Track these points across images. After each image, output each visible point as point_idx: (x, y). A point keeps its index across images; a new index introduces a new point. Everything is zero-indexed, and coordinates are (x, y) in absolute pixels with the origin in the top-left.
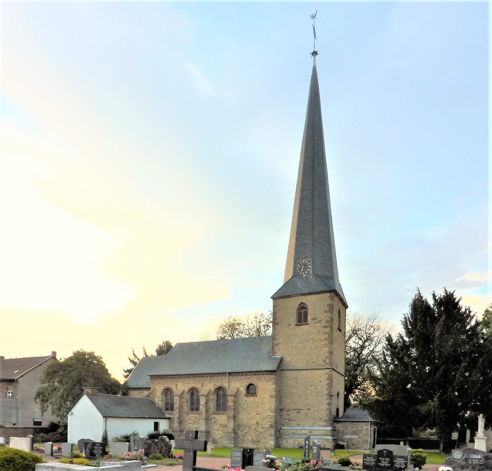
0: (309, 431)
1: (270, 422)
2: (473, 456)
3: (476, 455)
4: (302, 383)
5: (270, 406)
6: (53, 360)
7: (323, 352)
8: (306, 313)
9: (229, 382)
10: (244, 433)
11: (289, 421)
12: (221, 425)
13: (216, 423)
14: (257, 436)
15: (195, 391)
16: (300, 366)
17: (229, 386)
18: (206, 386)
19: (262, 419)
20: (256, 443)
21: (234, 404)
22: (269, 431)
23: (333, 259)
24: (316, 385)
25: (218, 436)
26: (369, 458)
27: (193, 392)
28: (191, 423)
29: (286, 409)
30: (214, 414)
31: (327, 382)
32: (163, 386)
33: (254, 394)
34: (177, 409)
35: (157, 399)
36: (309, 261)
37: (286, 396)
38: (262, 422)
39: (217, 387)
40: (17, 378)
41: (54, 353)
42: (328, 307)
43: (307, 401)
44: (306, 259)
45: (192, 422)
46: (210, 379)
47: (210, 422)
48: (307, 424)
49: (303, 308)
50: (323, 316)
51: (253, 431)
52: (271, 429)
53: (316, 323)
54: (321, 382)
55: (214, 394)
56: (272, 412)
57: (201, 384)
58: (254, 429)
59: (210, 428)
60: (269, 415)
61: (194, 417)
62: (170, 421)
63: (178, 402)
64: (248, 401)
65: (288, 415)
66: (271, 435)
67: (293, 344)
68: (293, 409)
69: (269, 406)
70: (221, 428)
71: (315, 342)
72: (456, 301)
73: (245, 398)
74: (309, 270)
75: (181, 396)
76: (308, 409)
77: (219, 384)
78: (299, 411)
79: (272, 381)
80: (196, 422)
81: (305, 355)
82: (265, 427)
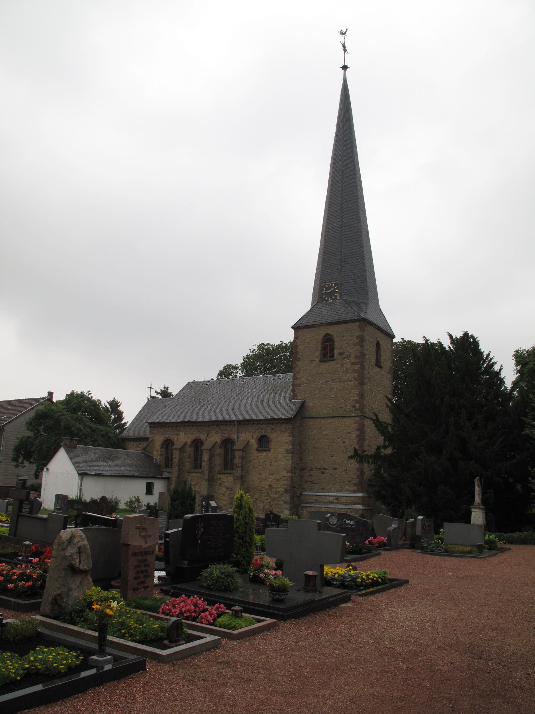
1: (284, 485)
4: (326, 435)
5: (286, 464)
6: (47, 403)
7: (352, 395)
8: (332, 347)
11: (312, 483)
12: (227, 488)
13: (222, 486)
14: (270, 503)
15: (199, 444)
17: (238, 438)
18: (211, 437)
19: (275, 480)
21: (242, 461)
23: (368, 280)
24: (344, 437)
27: (197, 444)
29: (308, 468)
30: (219, 473)
31: (358, 432)
32: (163, 436)
34: (176, 466)
36: (336, 284)
37: (308, 451)
38: (275, 485)
39: (224, 438)
40: (3, 424)
41: (51, 394)
42: (357, 339)
43: (333, 458)
44: (333, 281)
46: (217, 429)
47: (214, 484)
48: (333, 489)
50: (352, 351)
51: (264, 496)
53: (343, 359)
54: (349, 433)
55: (220, 447)
56: (287, 472)
57: (206, 435)
58: (266, 493)
59: (215, 491)
60: (283, 475)
61: (196, 477)
62: (168, 481)
63: (178, 457)
64: (259, 456)
65: (311, 476)
66: (285, 503)
69: (284, 463)
70: (228, 492)
71: (342, 383)
72: (123, 422)
73: (256, 454)
75: (182, 450)
77: (227, 434)
78: (324, 470)
79: (288, 431)
80: (198, 484)
81: (331, 398)
82: (280, 491)
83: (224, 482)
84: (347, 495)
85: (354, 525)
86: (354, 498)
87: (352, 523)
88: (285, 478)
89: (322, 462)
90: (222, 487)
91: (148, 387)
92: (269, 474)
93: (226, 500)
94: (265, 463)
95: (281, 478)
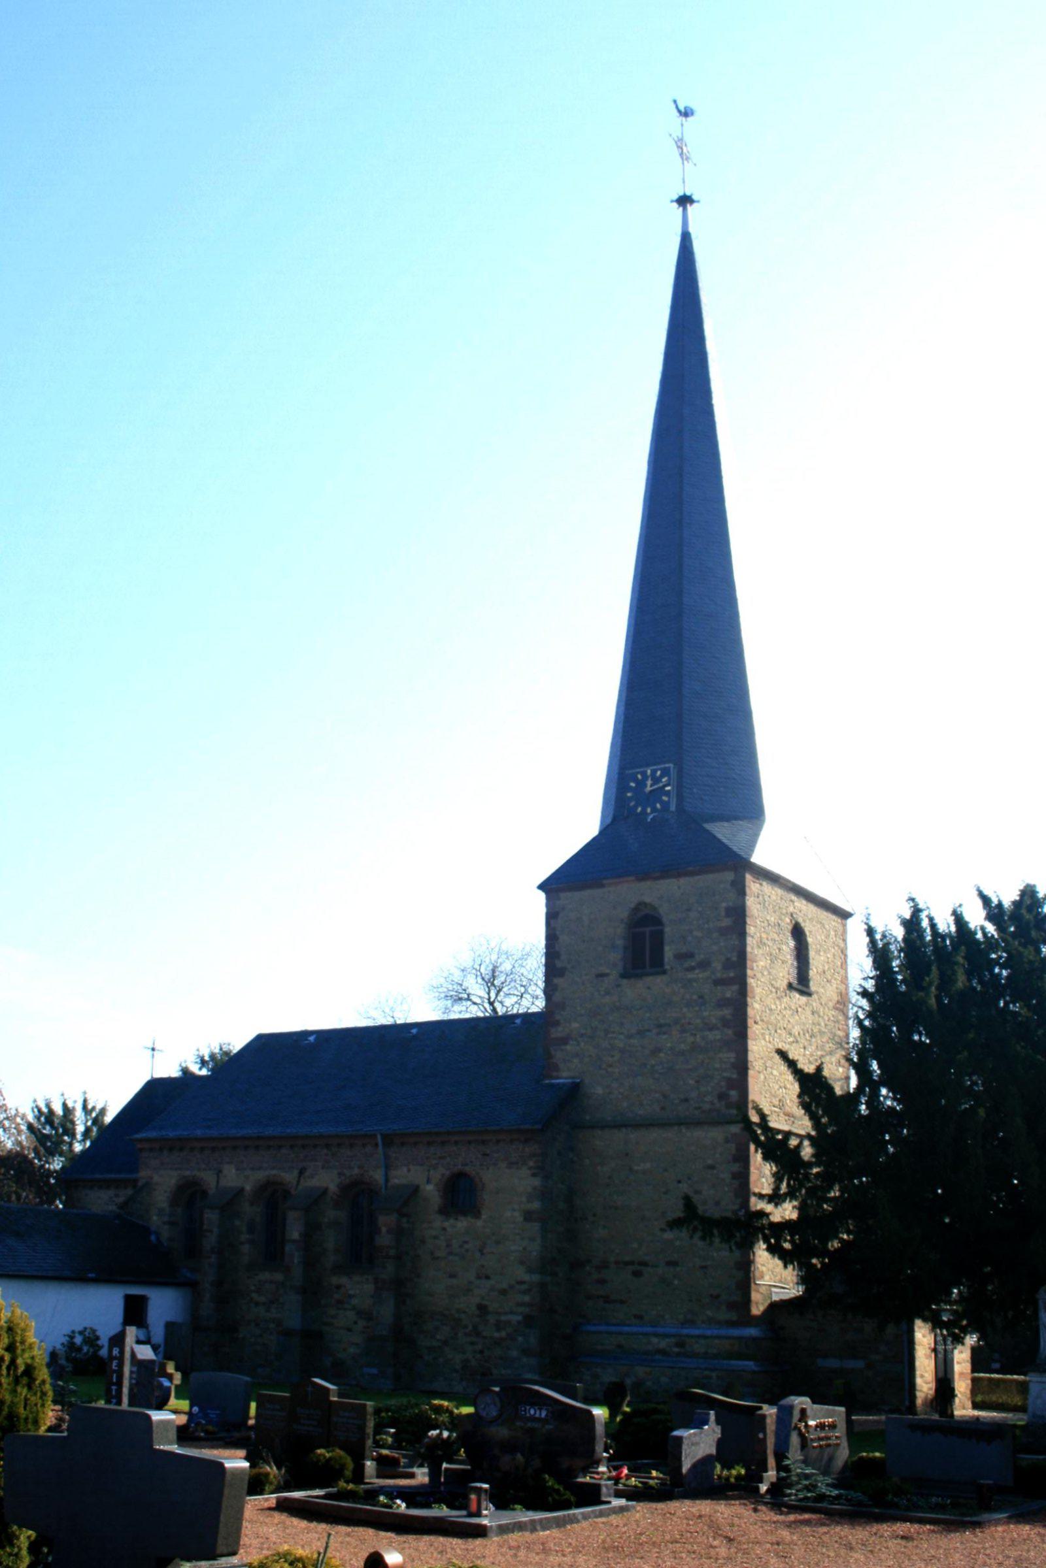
0: (673, 1340)
2: (527, 1411)
3: (536, 1408)
9: (387, 1168)
16: (641, 1112)
17: (387, 1181)
20: (479, 1377)
22: (520, 1339)
25: (352, 1350)
33: (472, 1209)
35: (155, 1218)
36: (665, 772)
53: (692, 969)
54: (712, 1167)
56: (530, 1271)
57: (296, 1173)
64: (449, 1229)
65: (602, 1282)
67: (615, 1038)
68: (617, 1263)
69: (521, 1249)
70: (362, 1323)
71: (688, 1034)
73: (438, 1222)
74: (665, 798)
76: (672, 1264)
77: (356, 1171)
79: (531, 1164)
84: (709, 1333)
89: (635, 1245)
92: (479, 1277)
93: (357, 1344)
94: (466, 1246)
95: (511, 1287)
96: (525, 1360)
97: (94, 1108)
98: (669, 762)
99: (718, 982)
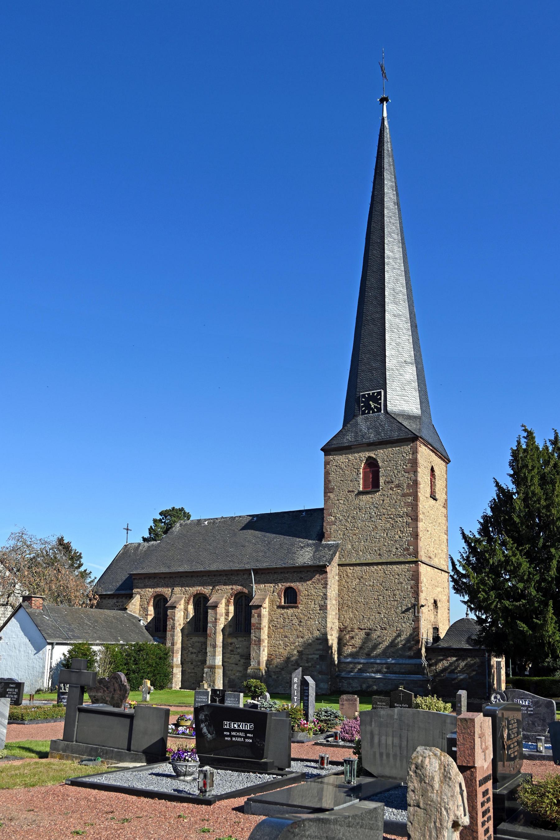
1: (318, 650)
10: (279, 670)
22: (318, 666)
26: (381, 703)
28: (195, 653)
45: (196, 651)
49: (372, 464)
51: (292, 665)
52: (321, 663)
61: (199, 642)
82: (313, 659)
83: (237, 648)
85: (532, 706)
86: (409, 666)
87: (527, 704)
88: (320, 641)
90: (235, 654)
91: (131, 530)
93: (240, 671)
96: (320, 676)
97: (78, 552)
98: (381, 389)
99: (404, 495)
